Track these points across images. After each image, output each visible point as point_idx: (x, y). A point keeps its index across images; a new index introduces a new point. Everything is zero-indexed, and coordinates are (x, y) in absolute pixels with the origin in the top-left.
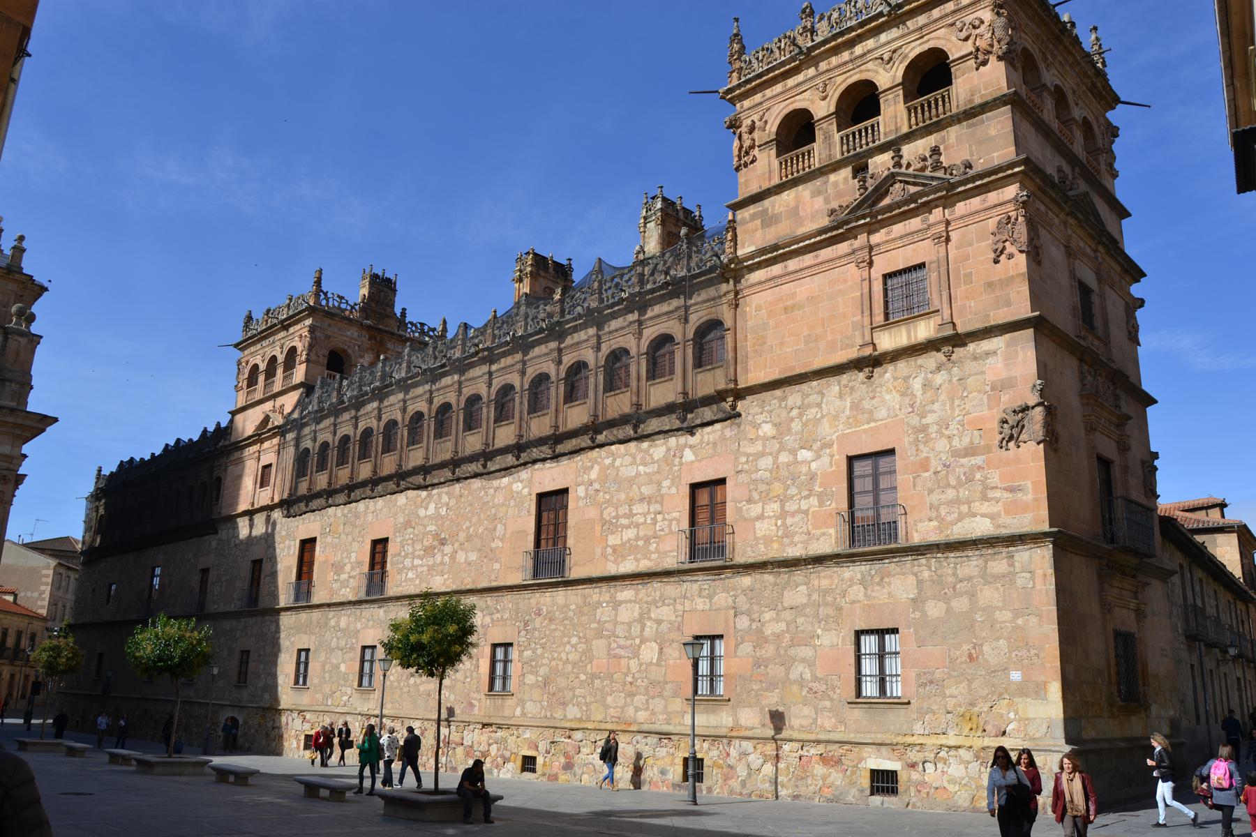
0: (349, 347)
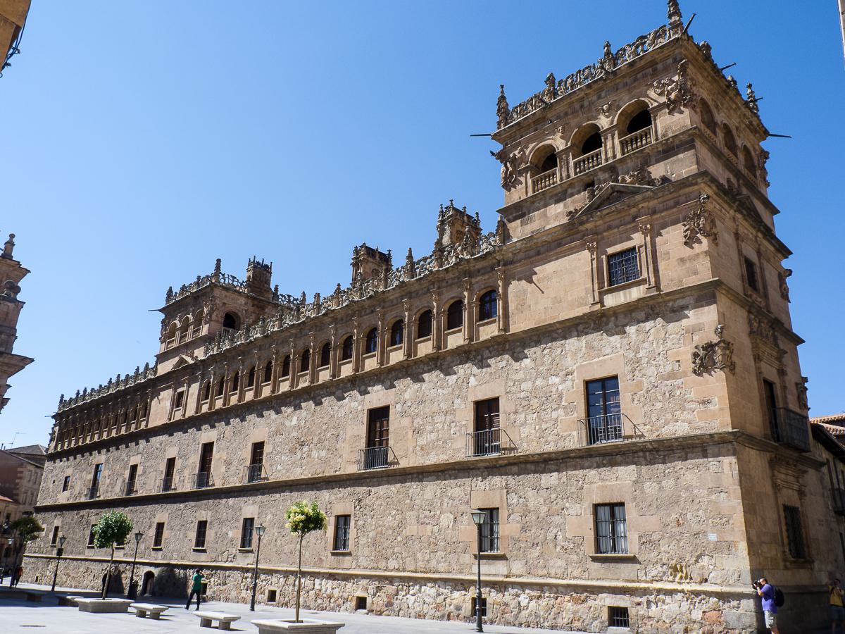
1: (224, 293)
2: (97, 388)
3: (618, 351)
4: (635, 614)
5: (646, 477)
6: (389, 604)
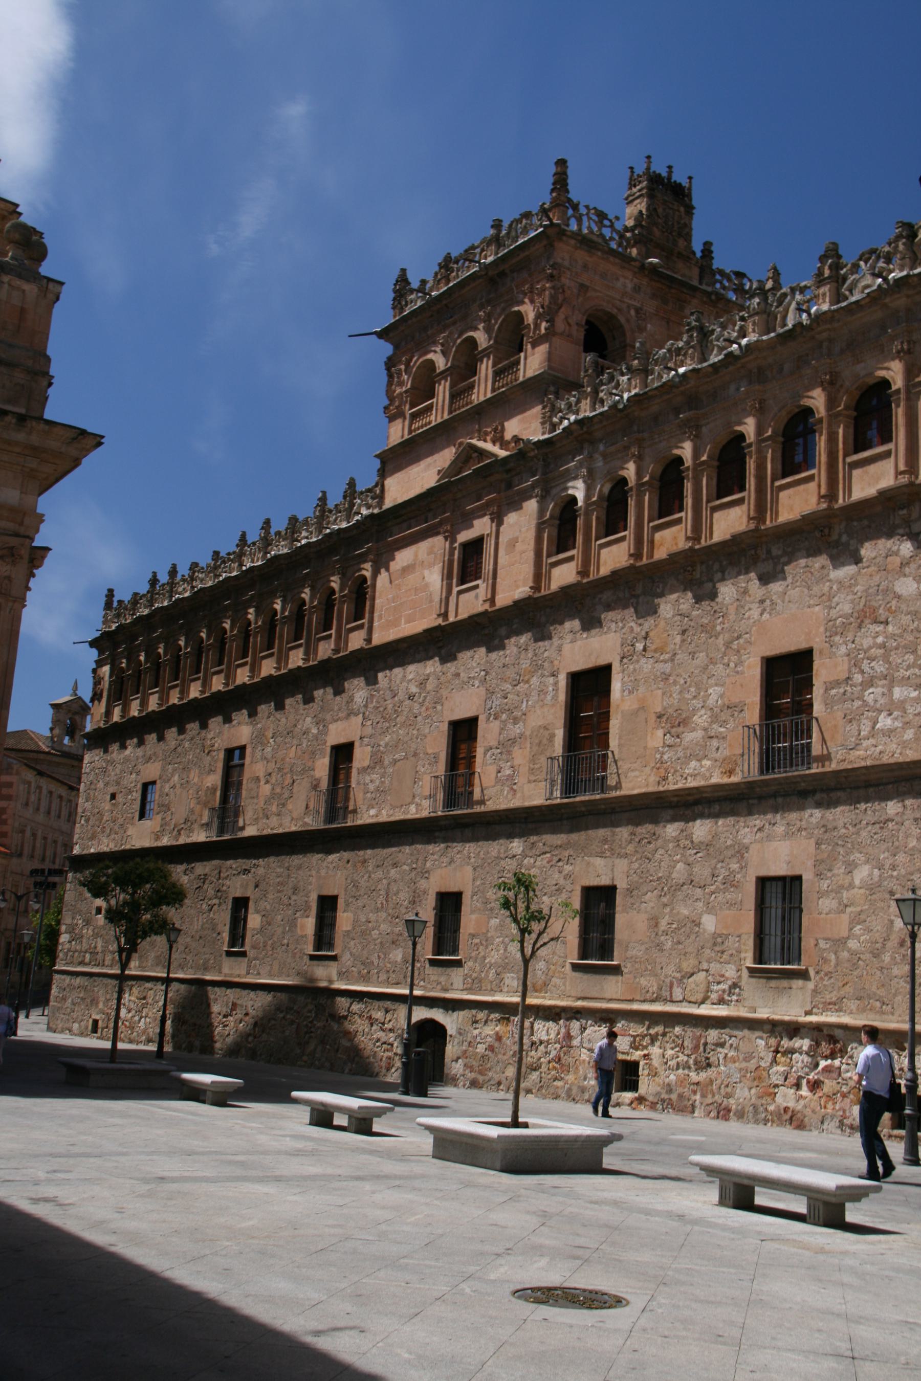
0: (619, 310)
1: (582, 256)
2: (205, 560)
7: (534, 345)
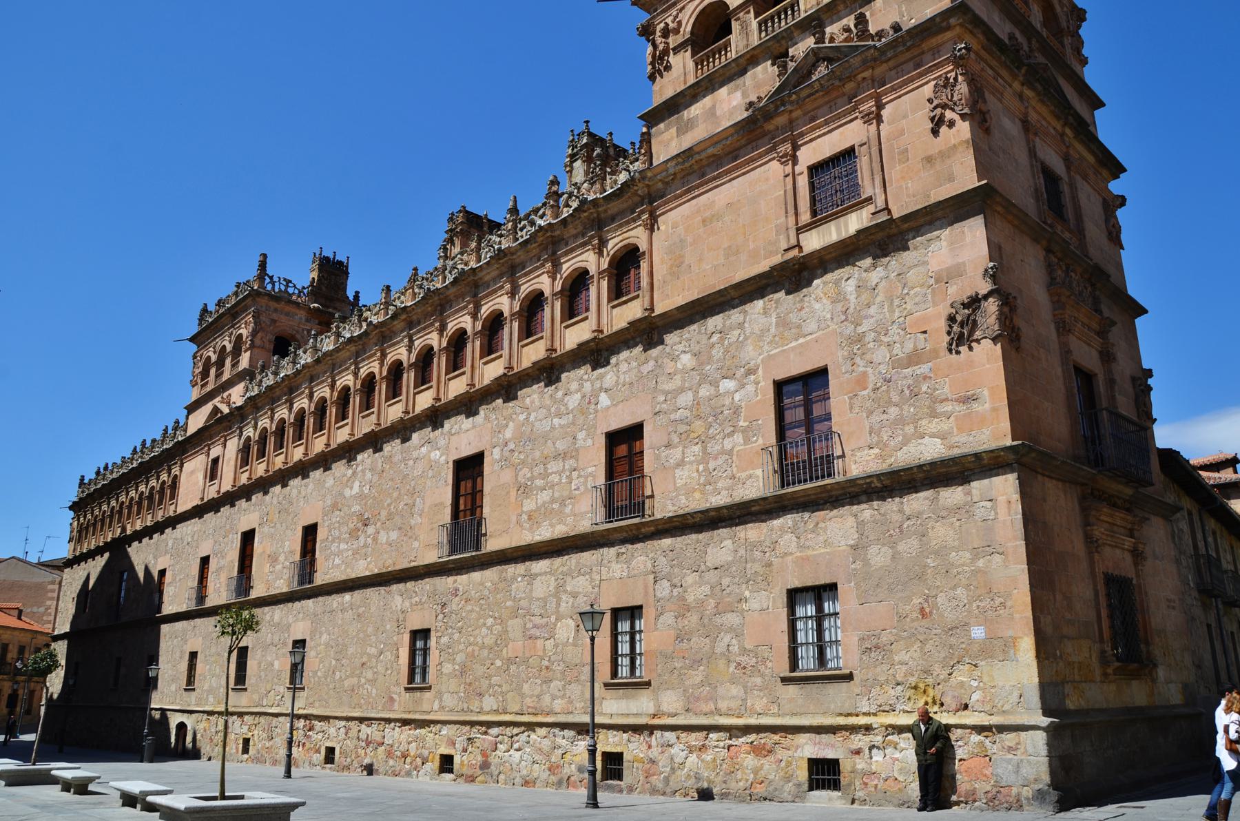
0: (297, 332)
1: (273, 304)
3: (829, 326)
4: (849, 769)
5: (872, 538)
6: (485, 766)
7: (245, 352)
